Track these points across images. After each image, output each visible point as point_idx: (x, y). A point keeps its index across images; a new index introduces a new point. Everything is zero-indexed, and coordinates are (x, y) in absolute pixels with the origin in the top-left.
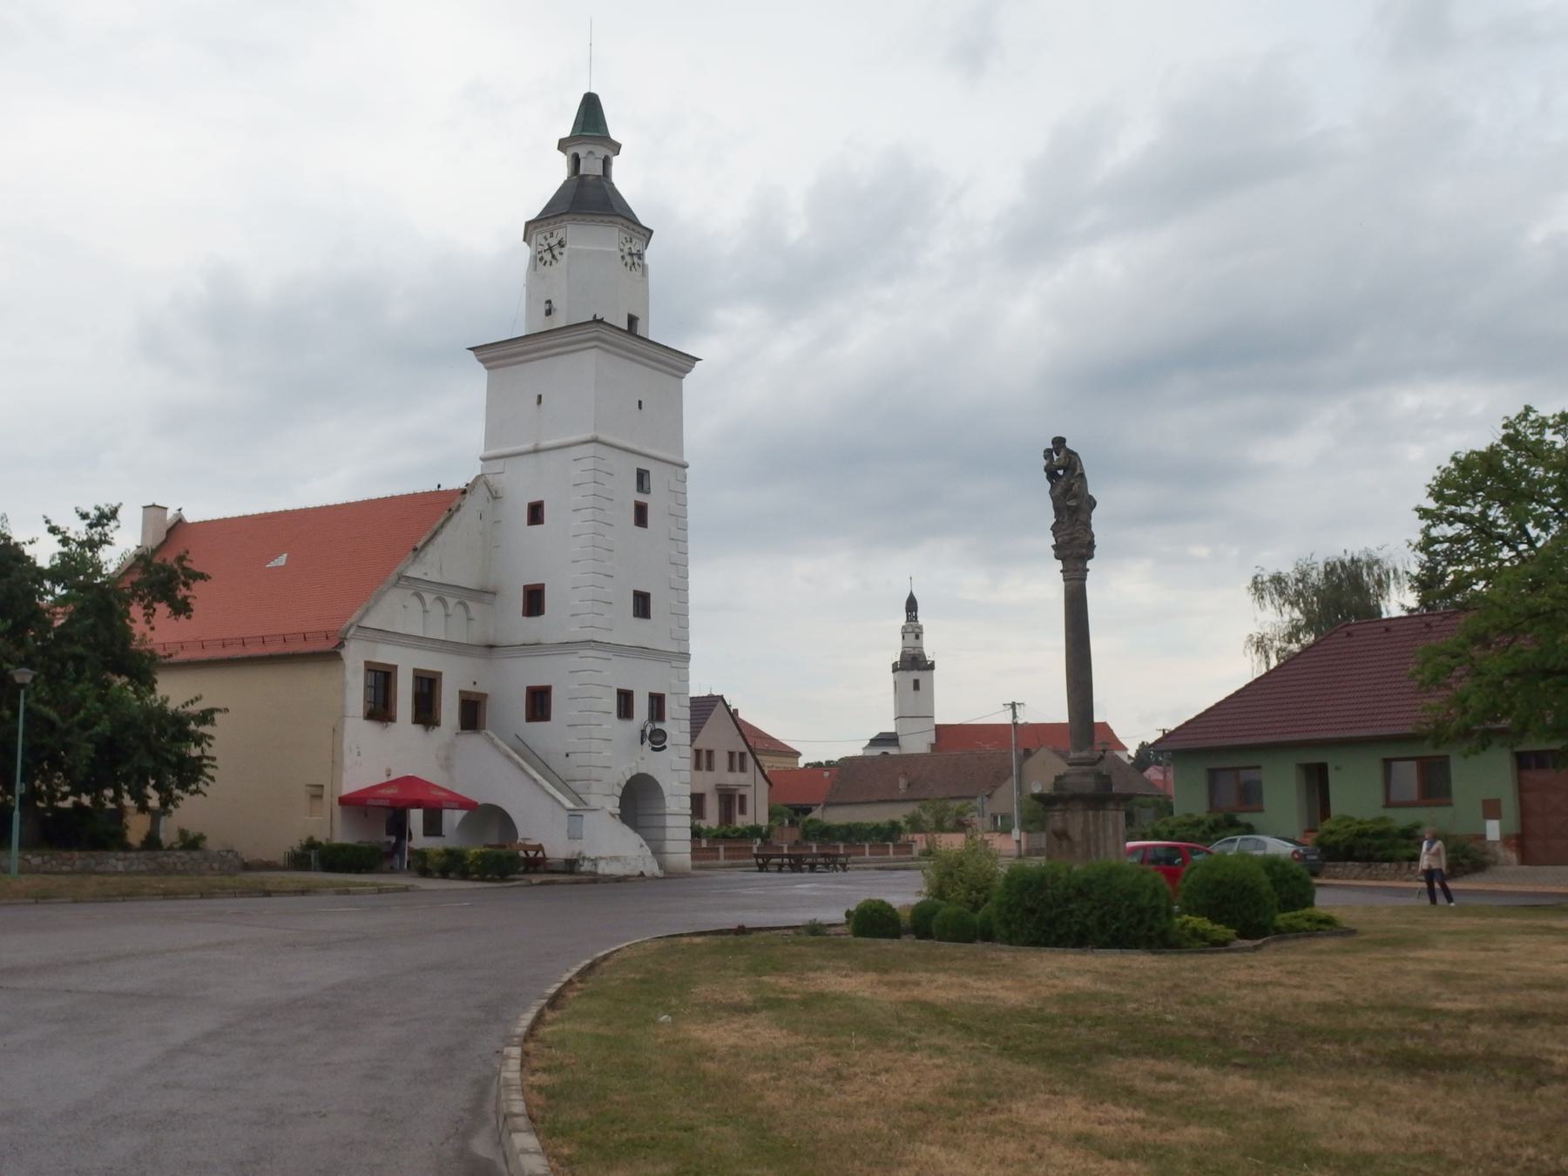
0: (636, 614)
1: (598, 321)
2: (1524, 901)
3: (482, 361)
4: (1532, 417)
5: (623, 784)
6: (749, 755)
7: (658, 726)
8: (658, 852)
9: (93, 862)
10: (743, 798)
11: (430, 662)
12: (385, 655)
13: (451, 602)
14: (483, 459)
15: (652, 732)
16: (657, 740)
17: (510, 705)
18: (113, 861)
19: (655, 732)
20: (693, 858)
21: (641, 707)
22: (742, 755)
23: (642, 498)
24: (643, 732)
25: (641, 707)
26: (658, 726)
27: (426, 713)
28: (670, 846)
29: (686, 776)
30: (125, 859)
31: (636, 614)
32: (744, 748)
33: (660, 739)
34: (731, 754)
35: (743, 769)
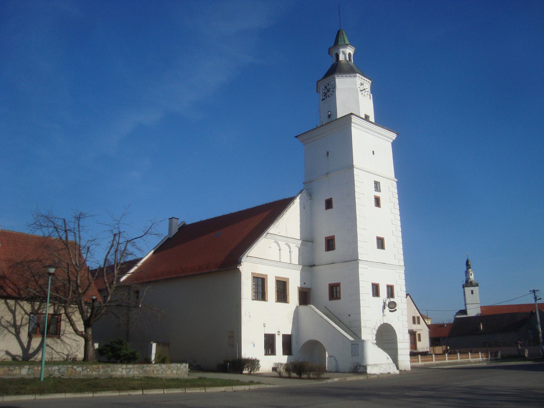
0: (378, 248)
1: (318, 81)
2: (416, 394)
3: (302, 141)
4: (52, 377)
5: (377, 328)
6: (421, 318)
7: (392, 300)
8: (395, 361)
9: (109, 370)
10: (419, 335)
11: (283, 274)
12: (261, 270)
13: (282, 244)
14: (304, 183)
15: (390, 303)
16: (392, 306)
17: (324, 292)
18: (120, 369)
19: (390, 303)
20: (411, 362)
21: (383, 291)
22: (418, 318)
23: (377, 194)
24: (385, 303)
25: (383, 291)
26: (392, 300)
27: (282, 295)
28: (400, 358)
29: (406, 324)
30: (127, 368)
31: (378, 248)
32: (419, 315)
33: (393, 306)
34: (414, 318)
35: (419, 323)
